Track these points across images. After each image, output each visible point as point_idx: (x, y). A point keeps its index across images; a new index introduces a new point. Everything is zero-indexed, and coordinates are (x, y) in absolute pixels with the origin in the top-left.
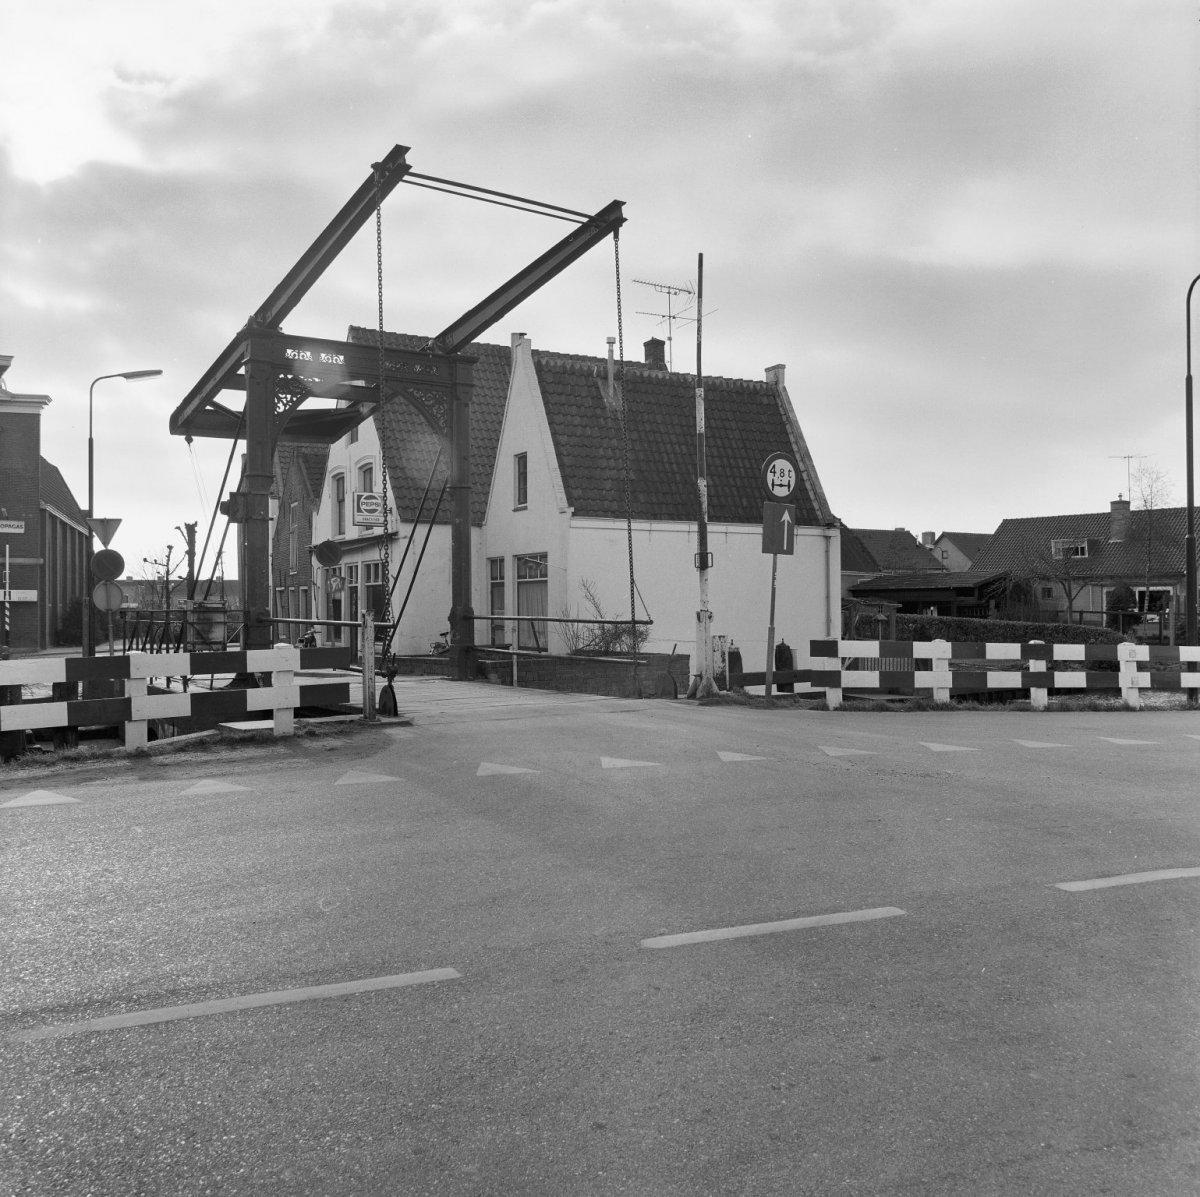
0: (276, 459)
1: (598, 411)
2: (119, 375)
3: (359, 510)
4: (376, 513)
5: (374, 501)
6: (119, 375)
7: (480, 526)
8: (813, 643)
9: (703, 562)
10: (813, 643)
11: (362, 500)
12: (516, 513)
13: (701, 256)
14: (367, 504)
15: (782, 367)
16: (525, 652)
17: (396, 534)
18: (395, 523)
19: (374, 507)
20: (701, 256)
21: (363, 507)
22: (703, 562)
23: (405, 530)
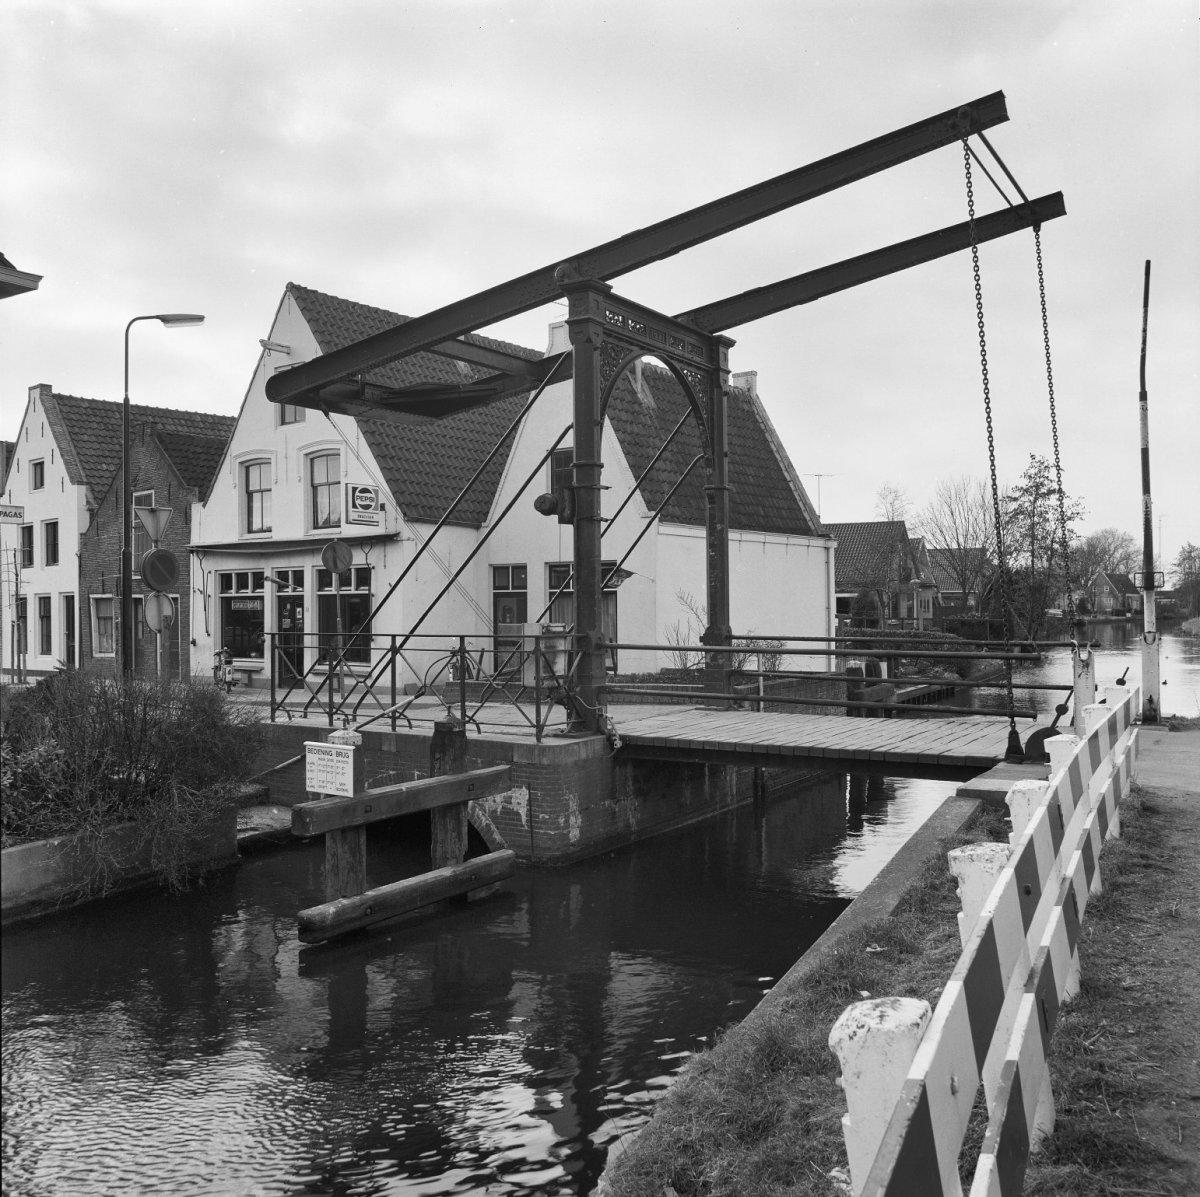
0: (661, 365)
1: (636, 407)
2: (157, 317)
3: (354, 506)
4: (370, 510)
5: (368, 495)
6: (157, 317)
7: (320, 571)
8: (1062, 212)
9: (607, 488)
10: (1062, 212)
11: (357, 493)
12: (392, 531)
13: (1148, 263)
14: (361, 498)
15: (753, 374)
16: (709, 694)
17: (397, 535)
18: (390, 519)
19: (368, 502)
20: (1148, 263)
21: (358, 502)
22: (607, 488)
23: (405, 530)
